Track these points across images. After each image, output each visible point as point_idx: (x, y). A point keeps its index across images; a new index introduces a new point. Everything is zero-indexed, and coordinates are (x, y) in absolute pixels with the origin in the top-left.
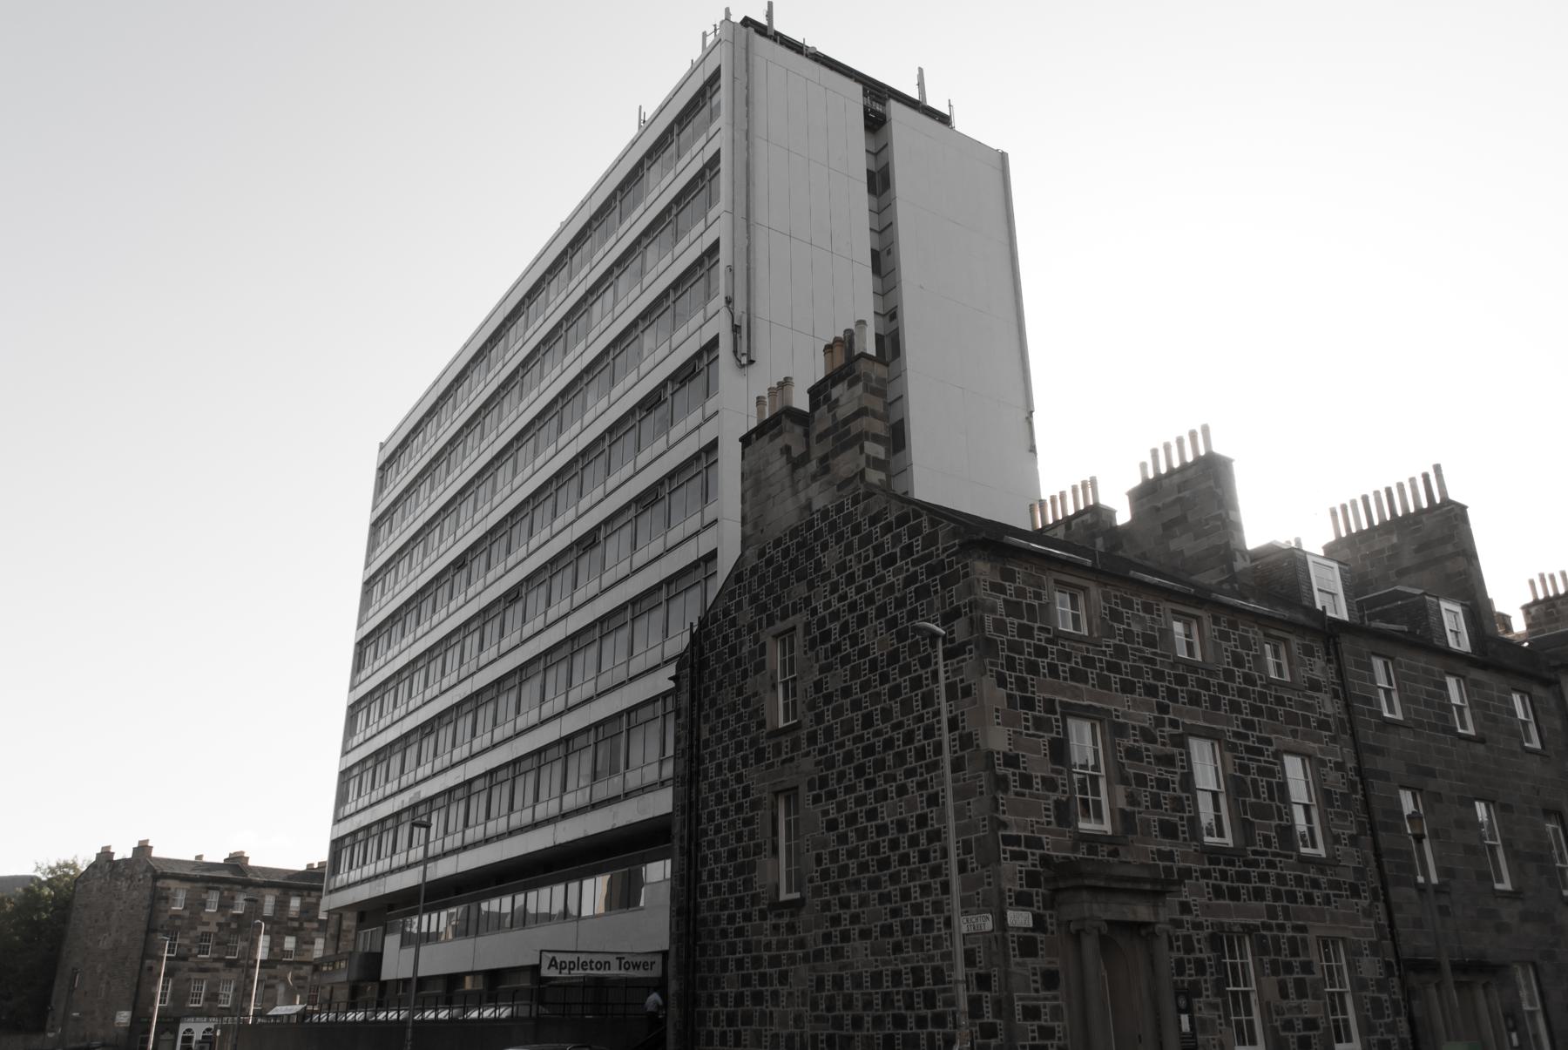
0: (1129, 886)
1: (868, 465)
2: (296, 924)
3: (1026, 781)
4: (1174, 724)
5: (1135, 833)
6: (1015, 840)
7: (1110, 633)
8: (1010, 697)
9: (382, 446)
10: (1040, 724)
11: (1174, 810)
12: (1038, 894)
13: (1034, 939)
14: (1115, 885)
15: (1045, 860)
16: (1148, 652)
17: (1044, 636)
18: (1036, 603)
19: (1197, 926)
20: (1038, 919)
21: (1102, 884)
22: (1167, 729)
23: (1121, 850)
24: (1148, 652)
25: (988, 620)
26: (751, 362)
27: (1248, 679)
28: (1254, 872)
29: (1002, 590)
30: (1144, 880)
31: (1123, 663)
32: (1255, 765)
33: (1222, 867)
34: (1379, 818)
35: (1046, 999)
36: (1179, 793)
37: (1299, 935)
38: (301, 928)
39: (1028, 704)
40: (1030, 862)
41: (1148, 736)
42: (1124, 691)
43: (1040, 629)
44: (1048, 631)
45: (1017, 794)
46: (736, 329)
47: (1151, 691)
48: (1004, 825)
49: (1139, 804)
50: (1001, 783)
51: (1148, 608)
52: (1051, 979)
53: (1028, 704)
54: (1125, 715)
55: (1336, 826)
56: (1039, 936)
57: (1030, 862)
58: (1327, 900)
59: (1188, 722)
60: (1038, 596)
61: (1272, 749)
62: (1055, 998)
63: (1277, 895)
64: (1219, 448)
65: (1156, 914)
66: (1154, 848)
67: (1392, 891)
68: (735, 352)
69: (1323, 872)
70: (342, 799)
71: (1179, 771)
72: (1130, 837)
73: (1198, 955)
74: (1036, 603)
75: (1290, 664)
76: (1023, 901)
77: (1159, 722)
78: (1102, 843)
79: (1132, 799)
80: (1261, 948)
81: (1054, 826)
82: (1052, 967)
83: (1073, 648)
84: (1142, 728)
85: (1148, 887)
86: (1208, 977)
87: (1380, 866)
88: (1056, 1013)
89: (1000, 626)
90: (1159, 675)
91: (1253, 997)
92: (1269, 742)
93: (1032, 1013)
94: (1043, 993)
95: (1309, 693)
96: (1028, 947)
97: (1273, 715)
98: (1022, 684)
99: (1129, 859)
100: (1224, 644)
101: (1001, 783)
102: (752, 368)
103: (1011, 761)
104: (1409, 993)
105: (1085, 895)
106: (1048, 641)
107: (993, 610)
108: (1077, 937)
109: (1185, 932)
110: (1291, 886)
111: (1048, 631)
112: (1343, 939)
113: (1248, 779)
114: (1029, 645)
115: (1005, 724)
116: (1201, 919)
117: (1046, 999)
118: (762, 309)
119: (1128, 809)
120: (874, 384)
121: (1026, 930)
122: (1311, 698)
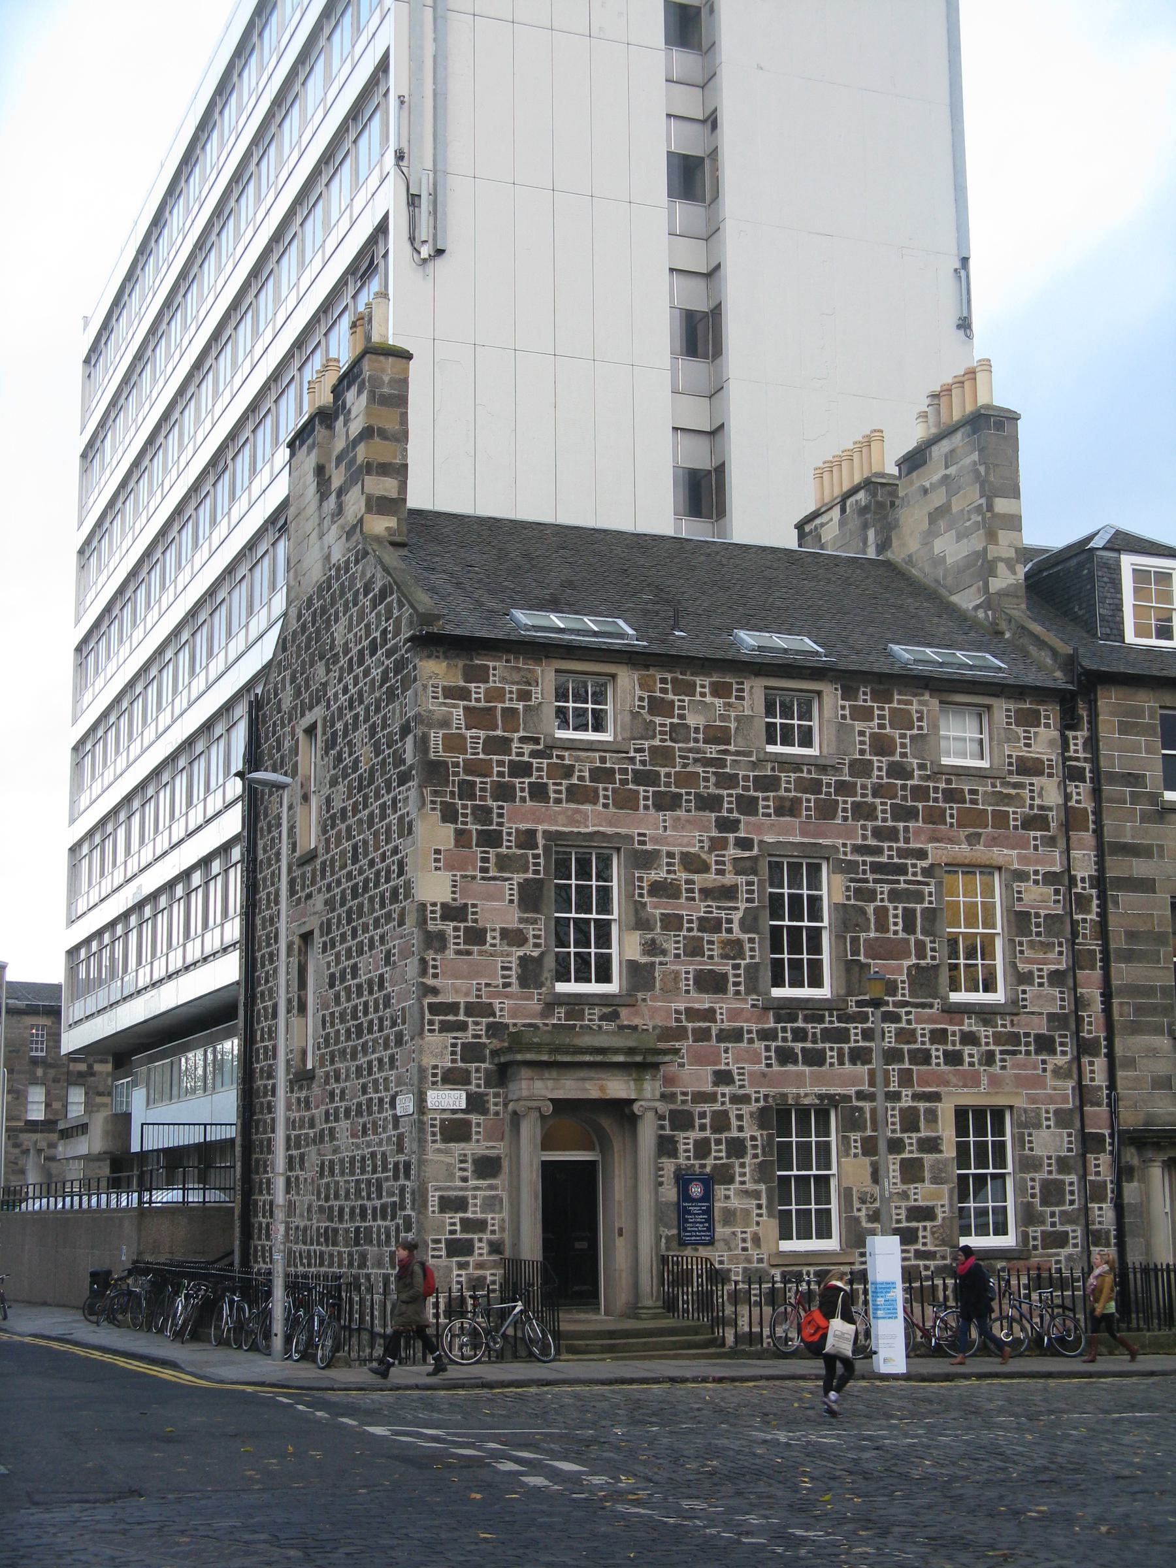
0: (587, 1058)
1: (369, 509)
2: (82, 1067)
3: (476, 936)
4: (744, 844)
5: (652, 988)
6: (453, 1008)
7: (649, 731)
8: (459, 833)
9: (86, 320)
10: (504, 863)
11: (725, 956)
12: (479, 1070)
13: (468, 1123)
14: (560, 1058)
15: (495, 1029)
16: (712, 751)
17: (527, 748)
18: (520, 706)
19: (744, 1099)
20: (476, 1103)
21: (545, 1058)
22: (732, 852)
23: (624, 1012)
24: (712, 751)
25: (436, 738)
26: (440, 252)
27: (899, 771)
28: (855, 1029)
29: (464, 694)
30: (616, 1051)
31: (663, 771)
32: (886, 888)
33: (800, 1024)
34: (1117, 943)
35: (477, 1188)
36: (737, 933)
37: (922, 1105)
38: (91, 1073)
39: (491, 839)
40: (470, 1033)
41: (693, 863)
42: (659, 807)
43: (522, 740)
44: (536, 741)
45: (458, 952)
46: (413, 200)
47: (709, 803)
48: (434, 991)
49: (664, 953)
50: (436, 941)
51: (720, 690)
52: (487, 1167)
53: (491, 839)
54: (655, 840)
55: (1029, 961)
56: (474, 1118)
57: (470, 1033)
58: (989, 1058)
59: (769, 839)
60: (524, 696)
61: (925, 864)
62: (492, 1187)
63: (892, 1056)
64: (1001, 393)
65: (640, 1090)
66: (682, 1006)
67: (1118, 1041)
68: (412, 239)
69: (986, 1023)
70: (73, 890)
71: (743, 906)
72: (640, 995)
73: (735, 1134)
74: (520, 706)
75: (991, 739)
76: (452, 1078)
77: (717, 845)
78: (592, 1005)
79: (652, 948)
80: (852, 1122)
81: (515, 988)
82: (493, 1153)
83: (578, 759)
84: (685, 855)
85: (621, 1058)
86: (748, 1160)
87: (1108, 1010)
88: (491, 1204)
89: (455, 743)
90: (729, 781)
91: (833, 1183)
92: (922, 854)
93: (451, 1204)
94: (472, 1183)
95: (1015, 779)
96: (455, 1130)
97: (934, 817)
98: (482, 815)
99: (637, 1021)
100: (858, 726)
101: (436, 941)
102: (440, 262)
103: (452, 912)
104: (1123, 1173)
105: (525, 1073)
106: (534, 754)
107: (445, 723)
108: (516, 1117)
109: (717, 1107)
110: (922, 1042)
111: (536, 741)
112: (1011, 1107)
113: (870, 908)
114: (501, 763)
115: (450, 867)
116: (748, 1090)
117: (477, 1188)
118: (458, 157)
119: (644, 960)
120: (386, 390)
121: (454, 1111)
122: (1016, 786)
